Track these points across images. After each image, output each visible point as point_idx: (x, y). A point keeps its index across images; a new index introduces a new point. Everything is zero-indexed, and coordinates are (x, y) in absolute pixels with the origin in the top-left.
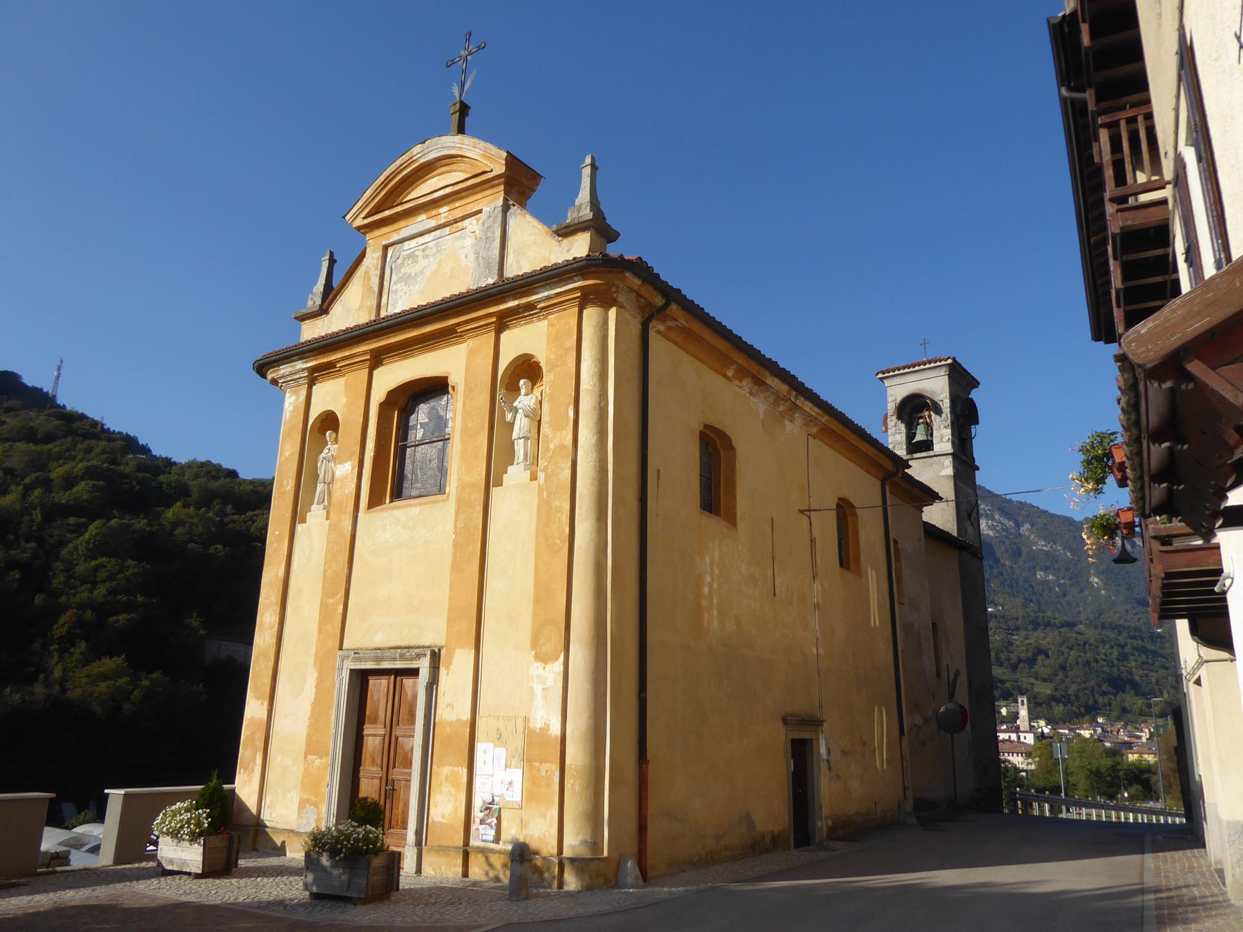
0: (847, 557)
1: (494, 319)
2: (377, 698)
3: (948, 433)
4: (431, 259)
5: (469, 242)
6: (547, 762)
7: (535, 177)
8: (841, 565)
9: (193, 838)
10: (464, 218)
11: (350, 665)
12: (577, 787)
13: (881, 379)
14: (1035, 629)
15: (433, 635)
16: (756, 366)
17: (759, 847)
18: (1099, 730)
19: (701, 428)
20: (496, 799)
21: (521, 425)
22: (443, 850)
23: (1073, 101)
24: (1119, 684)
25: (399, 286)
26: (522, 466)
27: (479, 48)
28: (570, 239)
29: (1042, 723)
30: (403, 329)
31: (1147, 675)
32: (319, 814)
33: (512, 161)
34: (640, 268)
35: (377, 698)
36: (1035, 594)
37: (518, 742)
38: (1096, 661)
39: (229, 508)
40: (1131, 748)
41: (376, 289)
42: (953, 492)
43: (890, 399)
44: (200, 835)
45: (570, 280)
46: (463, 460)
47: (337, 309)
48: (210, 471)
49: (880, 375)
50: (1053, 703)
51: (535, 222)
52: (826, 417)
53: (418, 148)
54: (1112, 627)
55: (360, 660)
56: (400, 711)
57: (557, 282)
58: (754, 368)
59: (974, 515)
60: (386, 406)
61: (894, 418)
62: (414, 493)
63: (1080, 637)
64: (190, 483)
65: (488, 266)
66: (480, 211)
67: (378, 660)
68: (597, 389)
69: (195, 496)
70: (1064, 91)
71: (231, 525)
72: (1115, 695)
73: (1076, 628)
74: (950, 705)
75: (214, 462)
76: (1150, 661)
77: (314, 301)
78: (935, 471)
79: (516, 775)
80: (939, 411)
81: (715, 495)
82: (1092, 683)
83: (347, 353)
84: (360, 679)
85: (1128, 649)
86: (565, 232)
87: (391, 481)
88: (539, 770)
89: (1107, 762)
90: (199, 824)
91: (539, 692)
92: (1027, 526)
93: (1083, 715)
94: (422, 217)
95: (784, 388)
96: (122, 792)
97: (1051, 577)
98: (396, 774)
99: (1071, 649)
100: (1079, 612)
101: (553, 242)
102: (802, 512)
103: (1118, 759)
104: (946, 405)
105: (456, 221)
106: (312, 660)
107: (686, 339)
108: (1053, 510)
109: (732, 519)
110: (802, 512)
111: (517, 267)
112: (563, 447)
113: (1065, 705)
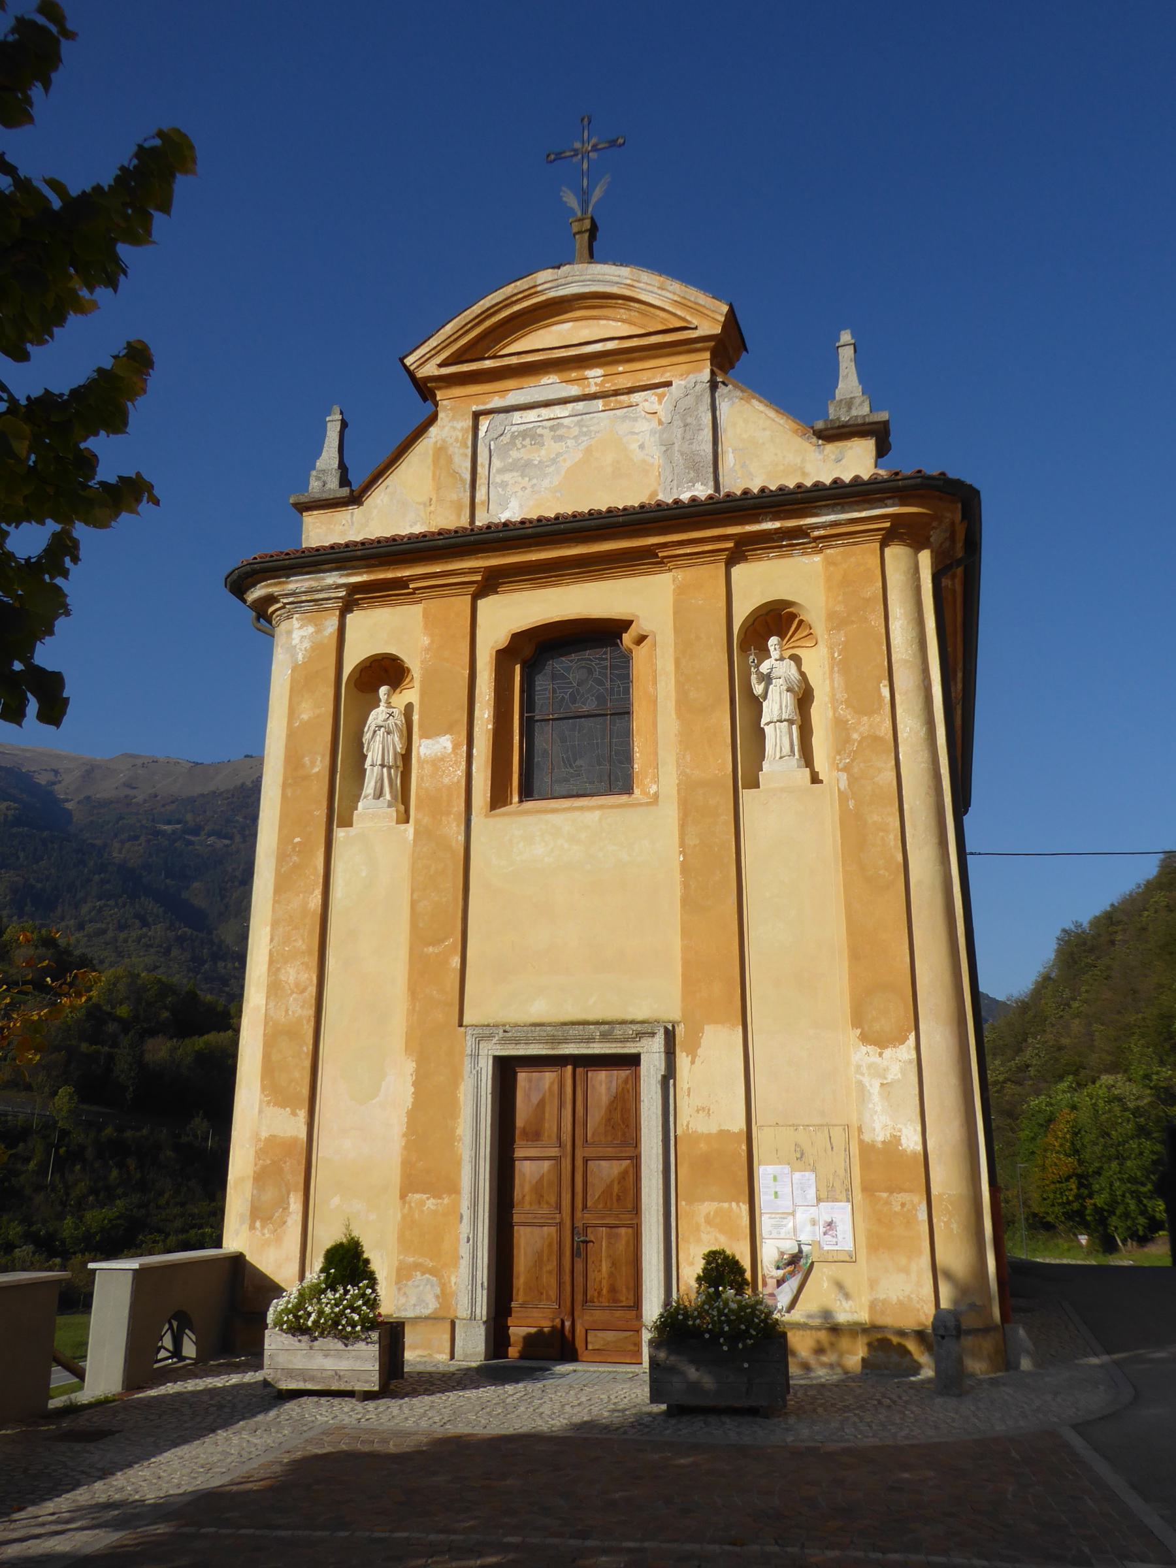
1: (730, 545)
4: (570, 443)
5: (645, 426)
10: (631, 391)
12: (954, 1226)
15: (654, 997)
20: (805, 1249)
21: (777, 706)
25: (507, 477)
27: (613, 143)
32: (443, 1286)
33: (731, 321)
47: (379, 498)
55: (517, 1042)
57: (857, 503)
60: (504, 657)
65: (693, 465)
66: (668, 384)
68: (918, 661)
79: (841, 1213)
83: (438, 569)
84: (506, 1070)
88: (887, 1203)
91: (874, 1087)
94: (552, 378)
96: (134, 1264)
105: (616, 393)
112: (876, 739)
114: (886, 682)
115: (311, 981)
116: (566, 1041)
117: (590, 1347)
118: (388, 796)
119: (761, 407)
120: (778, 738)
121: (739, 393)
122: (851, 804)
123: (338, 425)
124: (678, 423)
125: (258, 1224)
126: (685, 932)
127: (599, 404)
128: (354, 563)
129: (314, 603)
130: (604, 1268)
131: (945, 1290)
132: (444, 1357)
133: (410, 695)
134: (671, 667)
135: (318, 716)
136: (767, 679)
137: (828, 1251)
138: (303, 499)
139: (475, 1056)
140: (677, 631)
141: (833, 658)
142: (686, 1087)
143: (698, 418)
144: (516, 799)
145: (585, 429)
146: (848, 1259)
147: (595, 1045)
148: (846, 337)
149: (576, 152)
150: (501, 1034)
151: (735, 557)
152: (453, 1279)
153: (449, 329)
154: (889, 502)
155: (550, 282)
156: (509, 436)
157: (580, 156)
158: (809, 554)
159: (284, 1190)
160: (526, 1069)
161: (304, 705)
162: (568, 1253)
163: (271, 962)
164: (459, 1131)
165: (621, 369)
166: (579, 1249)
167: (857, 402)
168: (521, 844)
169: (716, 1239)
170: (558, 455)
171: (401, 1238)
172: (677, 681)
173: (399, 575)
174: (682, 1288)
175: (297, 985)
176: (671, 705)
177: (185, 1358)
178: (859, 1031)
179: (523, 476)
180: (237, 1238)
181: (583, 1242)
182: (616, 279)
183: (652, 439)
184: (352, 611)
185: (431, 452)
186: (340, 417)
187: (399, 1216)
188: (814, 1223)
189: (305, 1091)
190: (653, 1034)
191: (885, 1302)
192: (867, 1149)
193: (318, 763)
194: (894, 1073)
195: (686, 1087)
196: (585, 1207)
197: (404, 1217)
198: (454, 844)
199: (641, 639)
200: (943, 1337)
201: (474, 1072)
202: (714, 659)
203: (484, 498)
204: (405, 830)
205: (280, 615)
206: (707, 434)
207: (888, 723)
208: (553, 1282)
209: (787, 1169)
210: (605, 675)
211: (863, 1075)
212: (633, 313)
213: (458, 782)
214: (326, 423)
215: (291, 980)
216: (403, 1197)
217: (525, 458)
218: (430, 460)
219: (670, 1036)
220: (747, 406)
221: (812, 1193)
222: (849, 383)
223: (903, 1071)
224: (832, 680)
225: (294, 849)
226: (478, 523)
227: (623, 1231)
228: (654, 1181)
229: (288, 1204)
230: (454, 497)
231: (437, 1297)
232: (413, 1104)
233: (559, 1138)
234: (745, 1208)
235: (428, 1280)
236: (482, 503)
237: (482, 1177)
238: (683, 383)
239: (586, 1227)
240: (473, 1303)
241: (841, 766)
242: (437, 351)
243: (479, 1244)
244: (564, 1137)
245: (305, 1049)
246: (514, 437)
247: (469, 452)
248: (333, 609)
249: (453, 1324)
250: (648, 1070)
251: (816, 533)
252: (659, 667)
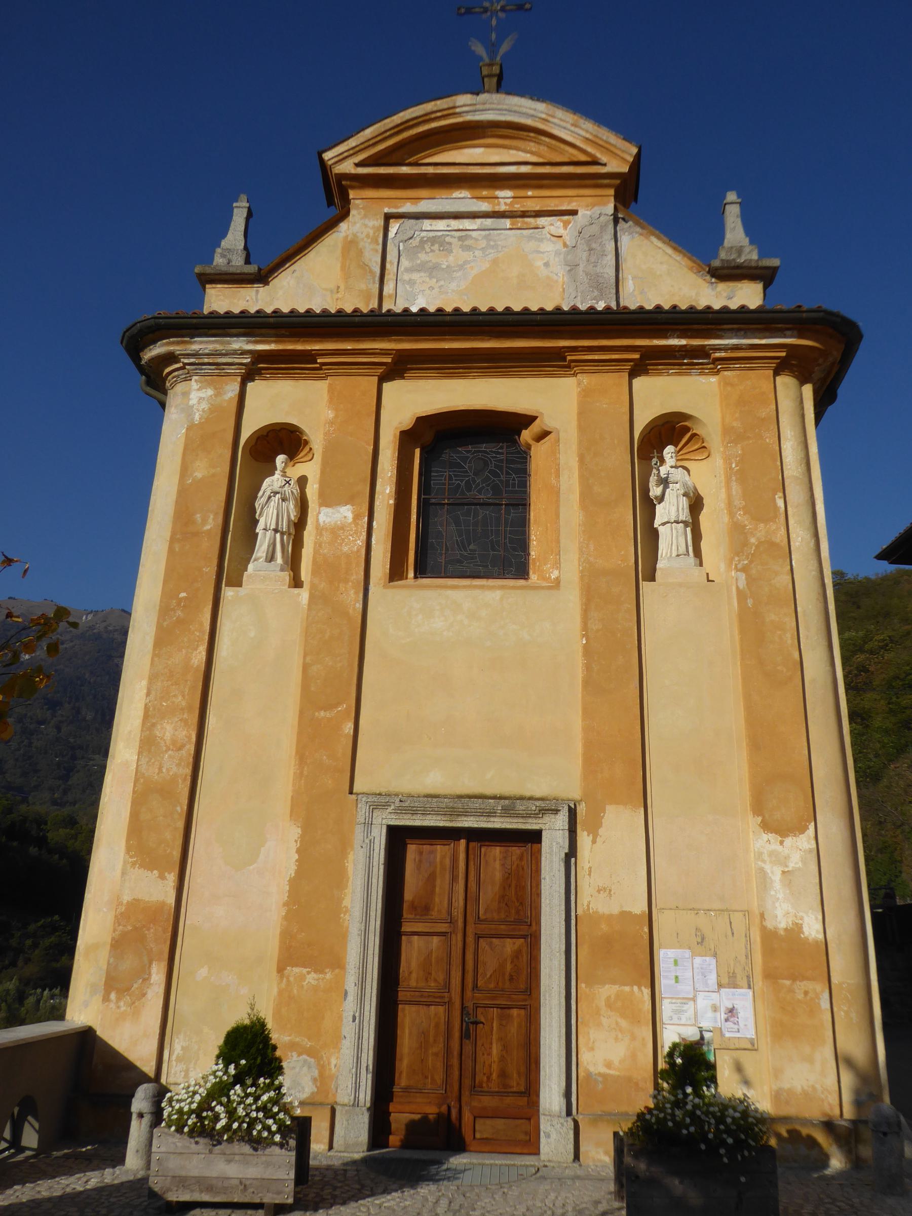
1: (636, 356)
4: (477, 253)
6: (804, 978)
10: (539, 214)
12: (853, 1015)
20: (707, 1035)
21: (670, 509)
25: (415, 276)
30: (444, 334)
32: (322, 1068)
41: (377, 270)
45: (780, 333)
53: (463, 100)
55: (414, 812)
60: (408, 438)
66: (574, 213)
67: (453, 813)
83: (349, 346)
88: (791, 990)
91: (776, 874)
105: (524, 214)
112: (772, 545)
114: (781, 494)
115: (189, 737)
116: (465, 813)
117: (478, 1136)
118: (279, 559)
119: (659, 244)
120: (671, 540)
121: (638, 229)
122: (750, 602)
123: (245, 213)
125: (113, 996)
126: (587, 712)
127: (507, 223)
128: (263, 331)
129: (215, 368)
130: (495, 1051)
131: (848, 1079)
133: (309, 468)
134: (574, 462)
135: (213, 475)
136: (665, 482)
137: (729, 1039)
138: (208, 270)
139: (368, 824)
140: (581, 429)
141: (731, 468)
142: (587, 866)
144: (411, 574)
145: (492, 243)
146: (749, 1046)
147: (496, 819)
148: (731, 196)
149: (486, 10)
150: (398, 804)
151: (638, 369)
152: (333, 1061)
153: (369, 132)
154: (788, 333)
156: (418, 239)
157: (489, 14)
158: (706, 374)
159: (145, 959)
160: (418, 841)
161: (198, 463)
162: (456, 1034)
163: (146, 716)
164: (347, 902)
165: (530, 193)
166: (468, 1029)
168: (420, 617)
169: (617, 1023)
170: (466, 262)
172: (581, 477)
173: (308, 347)
174: (582, 1074)
175: (174, 742)
176: (575, 496)
177: (23, 1149)
178: (760, 819)
179: (431, 277)
180: (83, 1008)
181: (472, 1023)
182: (532, 112)
183: (557, 259)
184: (253, 380)
185: (340, 245)
186: (247, 205)
187: (275, 991)
188: (715, 1009)
189: (177, 854)
190: (556, 811)
191: (790, 1092)
192: (769, 937)
193: (210, 521)
194: (795, 862)
195: (587, 866)
196: (475, 986)
197: (280, 993)
198: (351, 611)
199: (543, 435)
200: (885, 1134)
201: (367, 841)
202: (618, 459)
203: (392, 291)
204: (299, 595)
205: (178, 376)
206: (610, 259)
207: (783, 531)
208: (440, 1065)
209: (687, 953)
210: (501, 468)
211: (764, 861)
212: (542, 148)
213: (358, 551)
214: (233, 209)
215: (168, 736)
216: (280, 970)
217: (434, 261)
218: (339, 252)
220: (646, 241)
221: (712, 979)
222: (735, 234)
223: (804, 861)
224: (728, 488)
225: (179, 604)
227: (515, 1012)
228: (556, 962)
229: (150, 974)
230: (363, 286)
231: (315, 1080)
232: (297, 872)
233: (450, 913)
234: (647, 992)
235: (305, 1061)
236: (390, 296)
237: (370, 952)
238: (589, 213)
239: (476, 1007)
240: (357, 1088)
241: (740, 566)
242: (355, 151)
243: (366, 1024)
244: (455, 913)
245: (179, 809)
246: (423, 242)
247: (380, 248)
248: (235, 375)
249: (333, 1111)
250: (551, 847)
251: (717, 355)
252: (562, 462)
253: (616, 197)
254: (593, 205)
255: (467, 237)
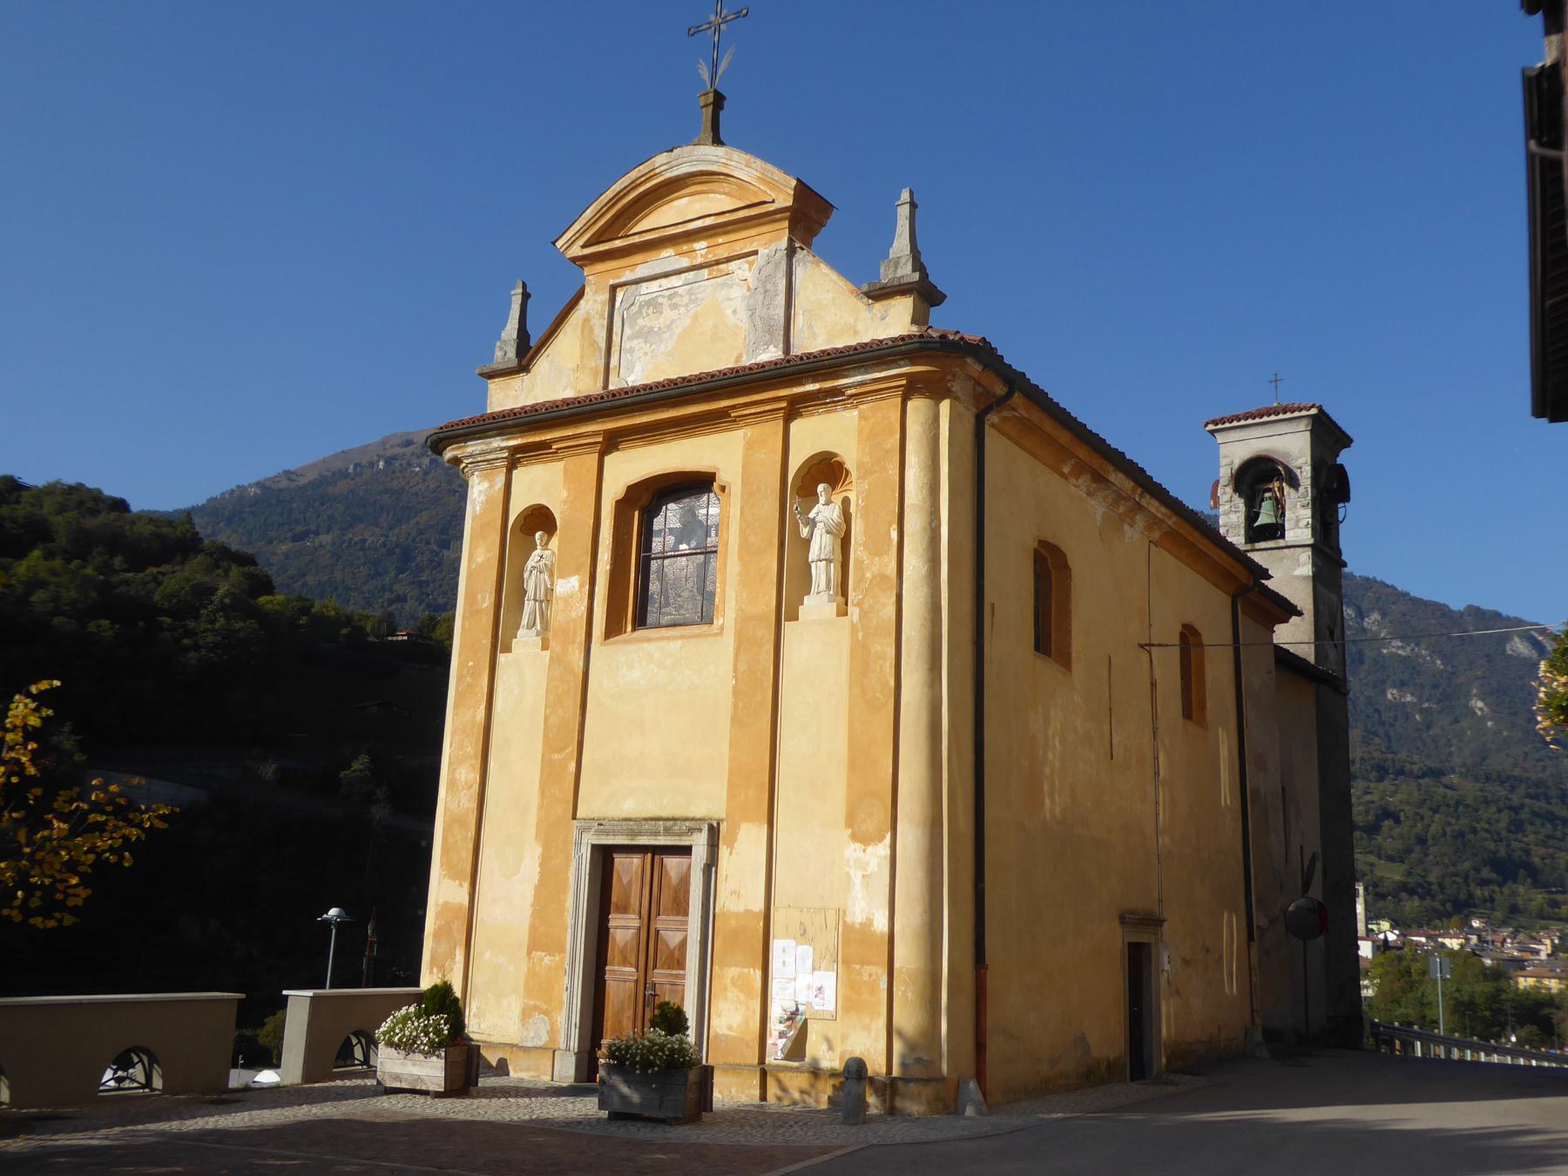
0: (1192, 706)
1: (784, 404)
2: (628, 882)
3: (1307, 513)
4: (682, 310)
5: (738, 292)
6: (869, 963)
7: (826, 208)
8: (1037, 648)
9: (434, 1048)
10: (729, 260)
11: (591, 839)
12: (909, 995)
13: (1212, 432)
14: (1380, 780)
15: (708, 801)
16: (1097, 459)
17: (1093, 1076)
18: (1474, 939)
19: (1035, 545)
20: (801, 1008)
21: (821, 545)
22: (735, 1068)
23: (1543, 159)
24: (1507, 869)
25: (634, 343)
26: (824, 597)
27: (738, 14)
28: (885, 303)
29: (1385, 925)
31: (1552, 857)
32: (552, 1024)
34: (984, 352)
35: (628, 882)
36: (1383, 724)
37: (830, 939)
38: (1474, 831)
39: (118, 561)
40: (1523, 968)
41: (603, 345)
42: (1310, 601)
43: (1223, 462)
44: (440, 1045)
46: (740, 583)
47: (542, 365)
48: (82, 500)
49: (1211, 427)
50: (1404, 895)
51: (834, 276)
52: (1174, 519)
53: (661, 159)
54: (1502, 779)
56: (665, 899)
58: (1096, 462)
59: (1337, 632)
60: (623, 506)
61: (1229, 490)
62: (665, 620)
63: (1450, 793)
64: (53, 519)
66: (755, 253)
67: (633, 833)
68: (927, 505)
69: (62, 541)
70: (1533, 144)
71: (123, 589)
72: (1500, 885)
73: (1445, 780)
74: (1301, 902)
75: (91, 484)
76: (1559, 834)
77: (505, 352)
78: (1290, 571)
79: (828, 979)
80: (1294, 483)
81: (1049, 635)
82: (1466, 865)
83: (569, 432)
84: (604, 857)
85: (1524, 815)
86: (879, 294)
87: (632, 604)
88: (860, 973)
89: (1483, 988)
90: (438, 1032)
92: (1375, 616)
93: (1449, 915)
94: (668, 252)
95: (1127, 484)
96: (310, 993)
97: (1409, 698)
98: (659, 975)
99: (1436, 811)
100: (1450, 754)
101: (860, 306)
102: (1142, 646)
103: (1503, 984)
104: (1305, 475)
105: (718, 263)
106: (532, 830)
107: (1023, 433)
108: (1415, 593)
109: (1065, 661)
110: (1142, 646)
111: (813, 338)
112: (883, 577)
113: (1422, 898)
116: (640, 833)
124: (761, 290)
126: (732, 745)
127: (705, 273)
131: (898, 1046)
132: (548, 1078)
143: (775, 285)
144: (629, 628)
153: (589, 213)
155: (667, 165)
167: (903, 260)
170: (673, 321)
171: (526, 986)
189: (468, 868)
192: (848, 928)
194: (873, 866)
206: (781, 299)
209: (793, 943)
216: (529, 953)
219: (714, 832)
226: (611, 387)
230: (593, 364)
234: (759, 973)
242: (581, 233)
253: (792, 230)
254: (771, 241)
255: (675, 294)
